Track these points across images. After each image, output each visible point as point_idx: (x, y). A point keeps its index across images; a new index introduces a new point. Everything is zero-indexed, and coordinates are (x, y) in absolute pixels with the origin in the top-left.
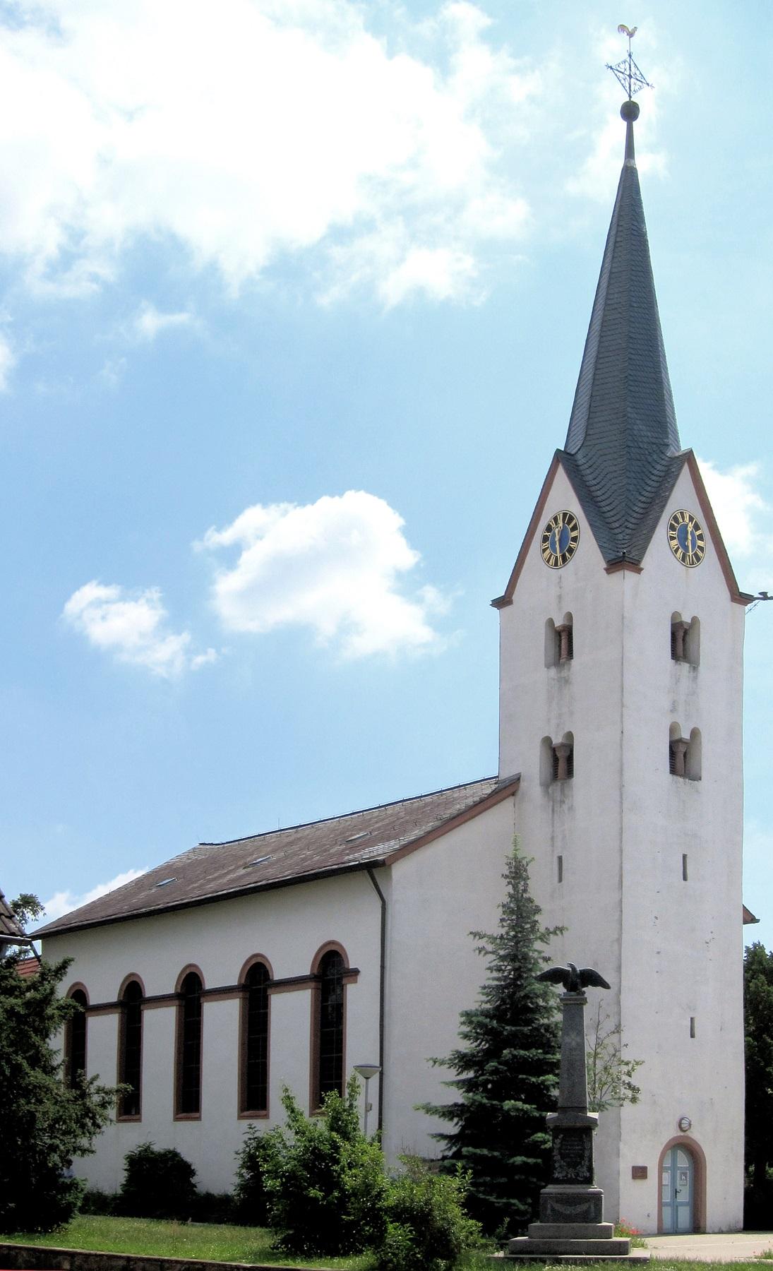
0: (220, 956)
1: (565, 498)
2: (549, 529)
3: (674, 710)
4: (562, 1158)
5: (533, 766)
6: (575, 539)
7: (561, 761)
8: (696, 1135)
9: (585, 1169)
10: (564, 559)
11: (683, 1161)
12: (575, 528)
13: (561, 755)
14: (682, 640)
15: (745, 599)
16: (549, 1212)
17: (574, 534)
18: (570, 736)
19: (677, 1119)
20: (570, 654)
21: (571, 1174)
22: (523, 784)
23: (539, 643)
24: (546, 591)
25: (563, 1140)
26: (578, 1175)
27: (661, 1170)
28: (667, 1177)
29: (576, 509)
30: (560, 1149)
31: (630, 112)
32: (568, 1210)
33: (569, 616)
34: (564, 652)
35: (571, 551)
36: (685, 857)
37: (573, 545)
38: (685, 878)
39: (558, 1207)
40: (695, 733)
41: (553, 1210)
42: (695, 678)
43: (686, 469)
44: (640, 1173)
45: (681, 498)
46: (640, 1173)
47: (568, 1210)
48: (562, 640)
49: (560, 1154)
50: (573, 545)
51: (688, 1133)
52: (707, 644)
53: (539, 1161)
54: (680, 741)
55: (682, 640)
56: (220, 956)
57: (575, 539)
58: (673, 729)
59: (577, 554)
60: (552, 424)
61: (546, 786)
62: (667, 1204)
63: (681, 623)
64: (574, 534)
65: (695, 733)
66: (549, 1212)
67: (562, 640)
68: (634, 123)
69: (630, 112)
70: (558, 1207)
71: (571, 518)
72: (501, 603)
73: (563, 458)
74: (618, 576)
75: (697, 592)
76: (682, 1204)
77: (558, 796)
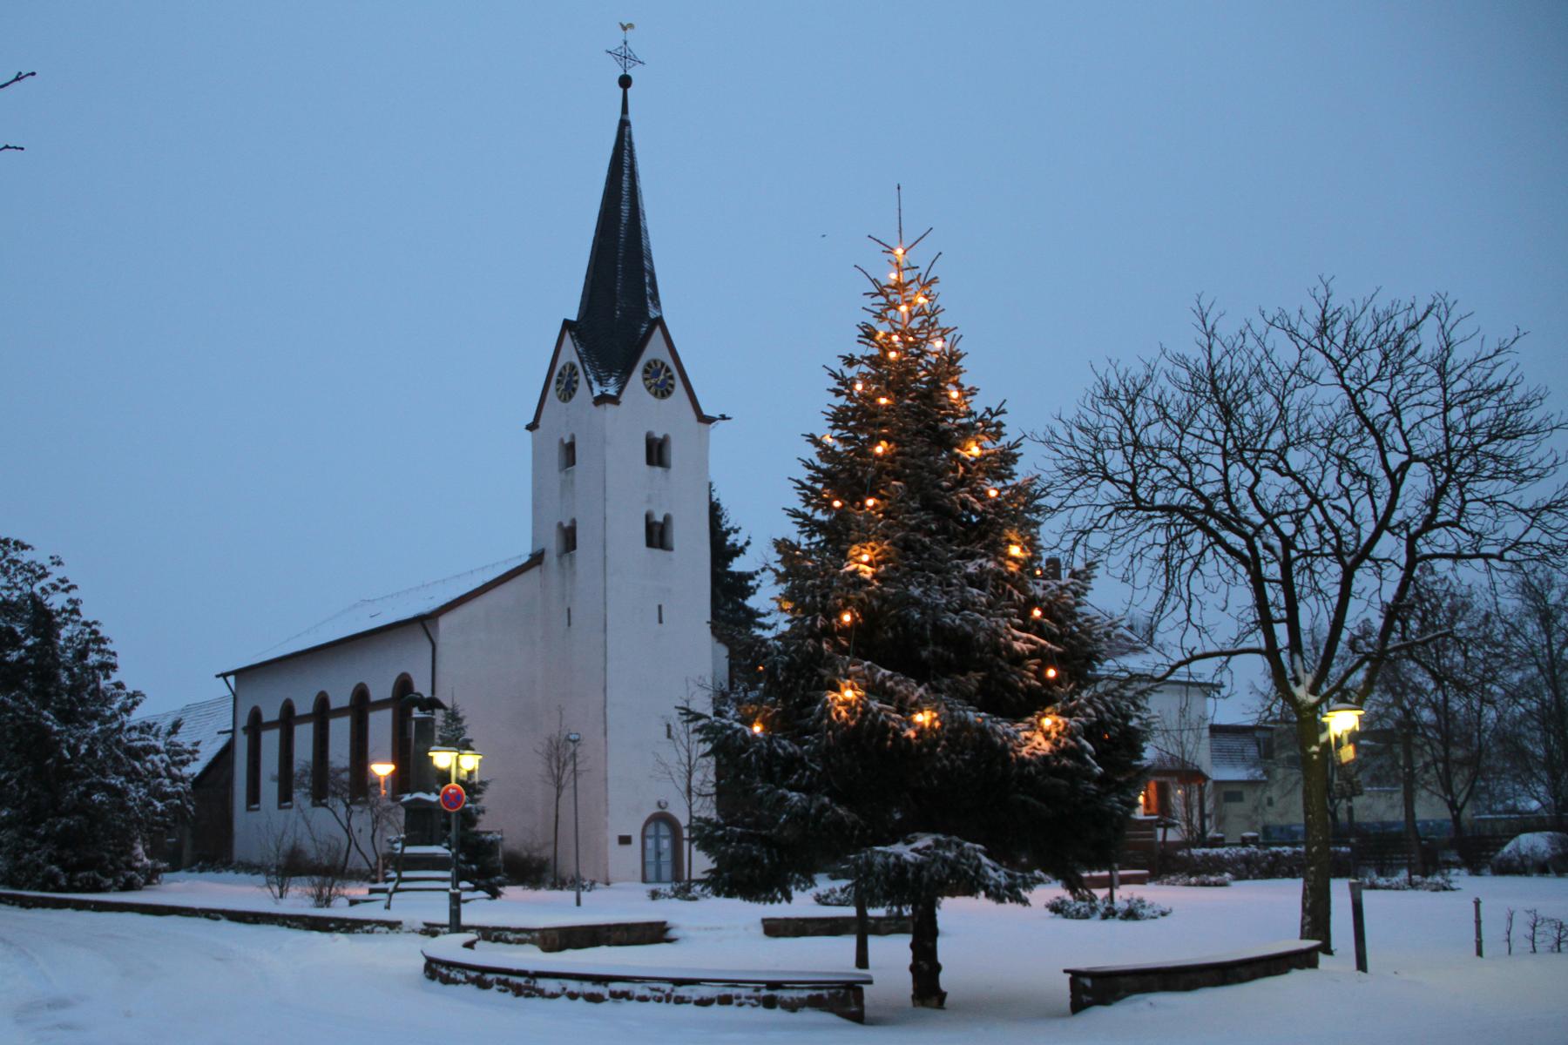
1: (570, 354)
2: (560, 374)
3: (649, 500)
5: (552, 543)
7: (569, 538)
11: (664, 830)
14: (656, 452)
15: (709, 420)
18: (574, 521)
22: (547, 557)
23: (554, 455)
24: (565, 418)
27: (644, 837)
28: (650, 843)
29: (576, 361)
31: (625, 82)
33: (573, 437)
36: (660, 607)
38: (661, 621)
40: (667, 518)
43: (658, 331)
44: (625, 840)
45: (655, 349)
46: (625, 840)
48: (569, 453)
52: (675, 454)
53: (1086, 875)
55: (656, 452)
58: (648, 517)
60: (567, 298)
61: (560, 556)
63: (655, 440)
67: (569, 453)
68: (629, 90)
69: (625, 82)
72: (532, 427)
73: (567, 325)
74: (601, 407)
75: (667, 417)
77: (567, 564)
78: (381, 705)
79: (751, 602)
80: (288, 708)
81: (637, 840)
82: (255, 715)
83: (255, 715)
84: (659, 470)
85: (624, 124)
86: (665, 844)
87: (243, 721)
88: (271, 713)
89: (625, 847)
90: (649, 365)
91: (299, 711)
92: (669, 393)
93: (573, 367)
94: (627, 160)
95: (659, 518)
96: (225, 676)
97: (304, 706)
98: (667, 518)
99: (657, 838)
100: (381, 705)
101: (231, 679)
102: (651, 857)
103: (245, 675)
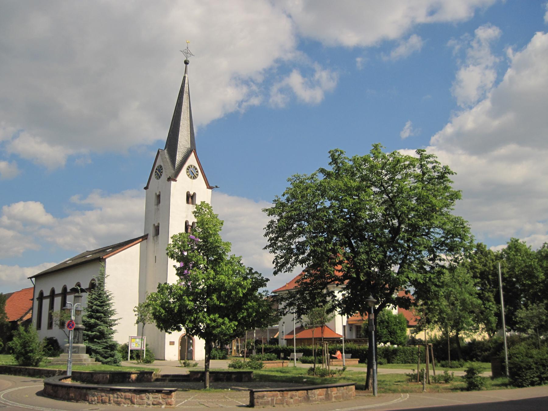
3: (187, 217)
31: (186, 63)
43: (193, 154)
54: (189, 225)
69: (186, 63)
79: (113, 318)
80: (53, 291)
82: (41, 293)
83: (41, 293)
87: (37, 295)
91: (45, 295)
95: (192, 193)
96: (31, 278)
98: (194, 194)
101: (33, 279)
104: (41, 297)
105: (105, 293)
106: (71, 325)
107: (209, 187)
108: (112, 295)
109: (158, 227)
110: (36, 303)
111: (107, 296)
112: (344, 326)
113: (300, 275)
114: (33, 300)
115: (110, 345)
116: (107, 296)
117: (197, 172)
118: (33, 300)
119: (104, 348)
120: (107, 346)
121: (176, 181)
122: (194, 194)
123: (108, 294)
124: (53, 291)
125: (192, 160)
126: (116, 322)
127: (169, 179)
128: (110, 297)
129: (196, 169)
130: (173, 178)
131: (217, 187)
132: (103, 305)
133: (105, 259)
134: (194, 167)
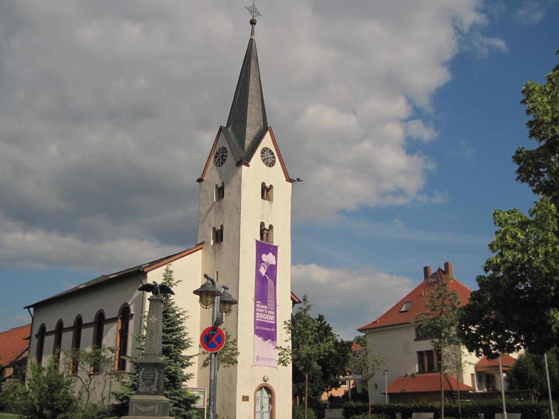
0: (87, 310)
1: (223, 142)
3: (262, 217)
4: (144, 381)
6: (226, 156)
8: (270, 383)
9: (155, 387)
10: (222, 163)
12: (226, 152)
13: (219, 234)
16: (134, 410)
17: (226, 154)
19: (263, 376)
20: (223, 197)
21: (148, 389)
25: (145, 371)
26: (151, 390)
29: (227, 146)
30: (142, 376)
31: (253, 23)
32: (143, 409)
34: (221, 196)
35: (224, 160)
37: (225, 158)
39: (139, 407)
40: (271, 227)
41: (136, 408)
42: (271, 207)
43: (268, 133)
44: (246, 398)
46: (246, 398)
47: (143, 409)
49: (142, 378)
50: (225, 158)
51: (267, 382)
54: (265, 229)
56: (87, 310)
57: (226, 156)
58: (262, 224)
59: (226, 161)
62: (258, 412)
64: (226, 154)
65: (271, 227)
66: (134, 410)
69: (253, 23)
70: (139, 407)
71: (225, 149)
76: (266, 412)
78: (88, 325)
79: (185, 353)
80: (60, 324)
81: (251, 399)
82: (43, 328)
83: (43, 328)
84: (267, 202)
85: (251, 41)
86: (266, 401)
87: (36, 331)
88: (51, 327)
89: (246, 395)
90: (264, 149)
91: (47, 330)
92: (273, 165)
93: (224, 149)
94: (253, 46)
95: (268, 185)
96: (28, 307)
97: (69, 323)
98: (271, 187)
99: (262, 397)
100: (88, 325)
101: (32, 310)
102: (258, 408)
103: (39, 307)
104: (42, 333)
105: (174, 311)
106: (213, 340)
107: (289, 180)
108: (186, 314)
109: (221, 230)
110: (35, 342)
111: (178, 316)
112: (472, 375)
113: (236, 340)
114: (29, 338)
115: (185, 399)
116: (178, 316)
117: (274, 157)
118: (29, 338)
119: (176, 405)
120: (180, 401)
121: (248, 166)
122: (271, 187)
123: (177, 312)
124: (60, 324)
125: (267, 142)
126: (191, 361)
127: (239, 164)
128: (181, 317)
129: (272, 154)
130: (244, 160)
131: (299, 180)
132: (171, 331)
133: (147, 272)
134: (270, 151)
